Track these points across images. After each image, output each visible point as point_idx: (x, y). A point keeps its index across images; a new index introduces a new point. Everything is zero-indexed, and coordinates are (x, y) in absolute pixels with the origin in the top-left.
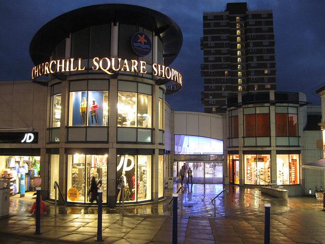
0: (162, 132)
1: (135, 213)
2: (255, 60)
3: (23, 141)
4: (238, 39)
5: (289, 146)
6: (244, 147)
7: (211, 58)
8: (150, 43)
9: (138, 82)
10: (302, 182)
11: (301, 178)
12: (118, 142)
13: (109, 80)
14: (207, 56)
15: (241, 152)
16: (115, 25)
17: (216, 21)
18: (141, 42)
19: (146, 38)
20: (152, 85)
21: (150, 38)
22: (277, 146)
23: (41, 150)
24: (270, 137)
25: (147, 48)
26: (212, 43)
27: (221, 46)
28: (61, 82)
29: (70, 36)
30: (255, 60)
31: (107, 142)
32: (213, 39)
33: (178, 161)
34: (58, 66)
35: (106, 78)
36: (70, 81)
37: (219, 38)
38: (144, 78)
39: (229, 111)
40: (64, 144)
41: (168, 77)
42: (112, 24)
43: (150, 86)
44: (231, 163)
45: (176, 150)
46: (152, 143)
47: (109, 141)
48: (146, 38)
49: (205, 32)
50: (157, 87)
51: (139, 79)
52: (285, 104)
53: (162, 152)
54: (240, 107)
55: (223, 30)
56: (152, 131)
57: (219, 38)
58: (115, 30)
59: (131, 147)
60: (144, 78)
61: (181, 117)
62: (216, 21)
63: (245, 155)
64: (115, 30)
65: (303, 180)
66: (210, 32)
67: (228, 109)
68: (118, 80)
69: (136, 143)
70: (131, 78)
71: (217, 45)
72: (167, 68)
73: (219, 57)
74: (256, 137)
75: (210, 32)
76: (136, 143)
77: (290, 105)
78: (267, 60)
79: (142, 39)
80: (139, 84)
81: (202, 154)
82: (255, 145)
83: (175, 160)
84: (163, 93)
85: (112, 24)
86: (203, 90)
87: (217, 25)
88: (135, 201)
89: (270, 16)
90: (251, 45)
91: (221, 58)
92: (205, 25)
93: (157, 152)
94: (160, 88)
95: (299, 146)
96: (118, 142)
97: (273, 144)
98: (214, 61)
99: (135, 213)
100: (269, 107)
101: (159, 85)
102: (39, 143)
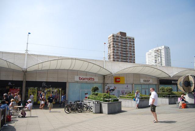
1: (58, 100)
2: (129, 54)
7: (115, 51)
23: (107, 113)
24: (177, 85)
26: (116, 46)
27: (119, 47)
30: (129, 54)
32: (116, 44)
37: (118, 45)
55: (119, 42)
57: (118, 45)
66: (115, 42)
75: (115, 42)
86: (155, 62)
87: (117, 39)
89: (134, 39)
90: (128, 49)
91: (131, 51)
99: (58, 100)
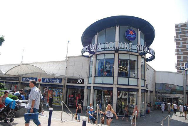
0: (143, 81)
3: (77, 83)
5: (103, 84)
6: (95, 84)
8: (135, 34)
12: (118, 85)
13: (114, 53)
14: (178, 45)
16: (118, 27)
17: (182, 28)
18: (131, 34)
19: (133, 32)
20: (137, 56)
21: (136, 32)
25: (134, 37)
26: (181, 39)
28: (93, 56)
29: (97, 34)
31: (113, 84)
32: (181, 36)
34: (90, 47)
35: (113, 52)
36: (97, 54)
38: (133, 52)
39: (186, 70)
42: (116, 26)
48: (133, 32)
49: (177, 33)
51: (130, 53)
57: (185, 36)
58: (117, 29)
59: (136, 88)
60: (133, 52)
62: (182, 28)
64: (117, 29)
66: (179, 33)
68: (119, 53)
69: (128, 85)
70: (126, 52)
71: (183, 40)
76: (128, 85)
78: (180, 27)
79: (131, 32)
82: (101, 82)
85: (116, 26)
92: (176, 30)
95: (137, 86)
97: (115, 83)
98: (182, 48)
101: (141, 55)
102: (37, 77)
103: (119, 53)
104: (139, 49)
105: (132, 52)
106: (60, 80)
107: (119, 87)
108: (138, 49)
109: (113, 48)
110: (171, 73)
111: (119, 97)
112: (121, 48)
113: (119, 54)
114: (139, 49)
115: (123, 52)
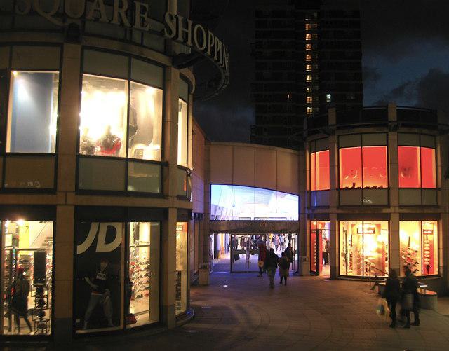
4: (308, 47)
5: (361, 134)
9: (130, 56)
10: (444, 271)
11: (441, 264)
12: (79, 192)
15: (395, 217)
20: (164, 66)
22: (401, 206)
24: (57, 205)
31: (53, 191)
33: (217, 232)
39: (311, 142)
40: (397, 208)
41: (201, 46)
43: (160, 70)
44: (314, 236)
45: (212, 213)
46: (162, 195)
47: (60, 188)
50: (175, 73)
52: (416, 131)
53: (185, 215)
54: (333, 133)
56: (162, 168)
59: (159, 206)
61: (223, 153)
63: (341, 223)
65: (444, 266)
67: (309, 139)
70: (115, 45)
72: (203, 49)
73: (92, 328)
74: (421, 189)
77: (425, 131)
80: (134, 61)
81: (252, 219)
83: (211, 231)
84: (189, 92)
88: (122, 327)
93: (172, 214)
94: (182, 77)
95: (162, 195)
96: (79, 192)
100: (387, 133)
101: (180, 67)
103: (83, 48)
104: (177, 35)
105: (141, 45)
106: (205, 150)
107: (85, 203)
108: (170, 33)
109: (57, 15)
110: (406, 190)
111: (81, 249)
112: (97, 20)
113: (389, 202)
114: (173, 36)
115: (102, 43)
